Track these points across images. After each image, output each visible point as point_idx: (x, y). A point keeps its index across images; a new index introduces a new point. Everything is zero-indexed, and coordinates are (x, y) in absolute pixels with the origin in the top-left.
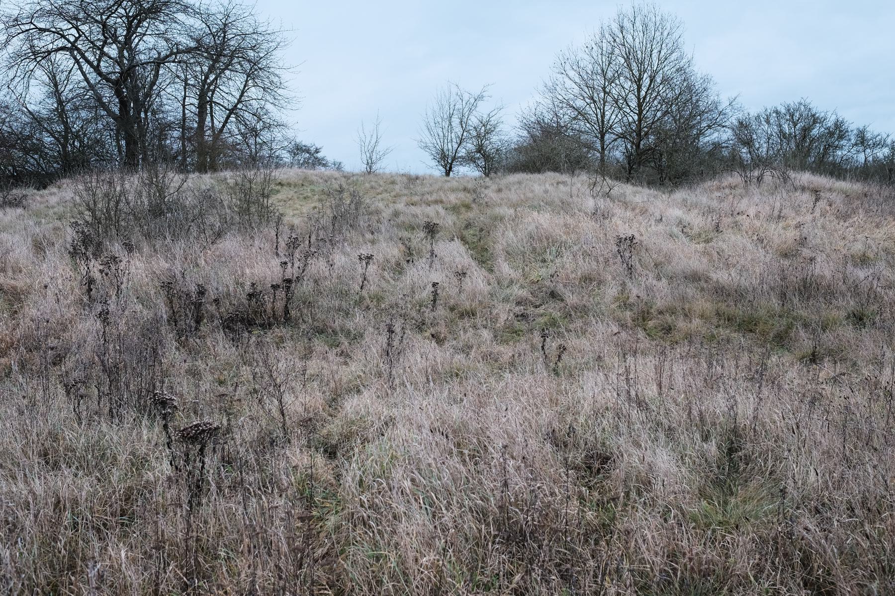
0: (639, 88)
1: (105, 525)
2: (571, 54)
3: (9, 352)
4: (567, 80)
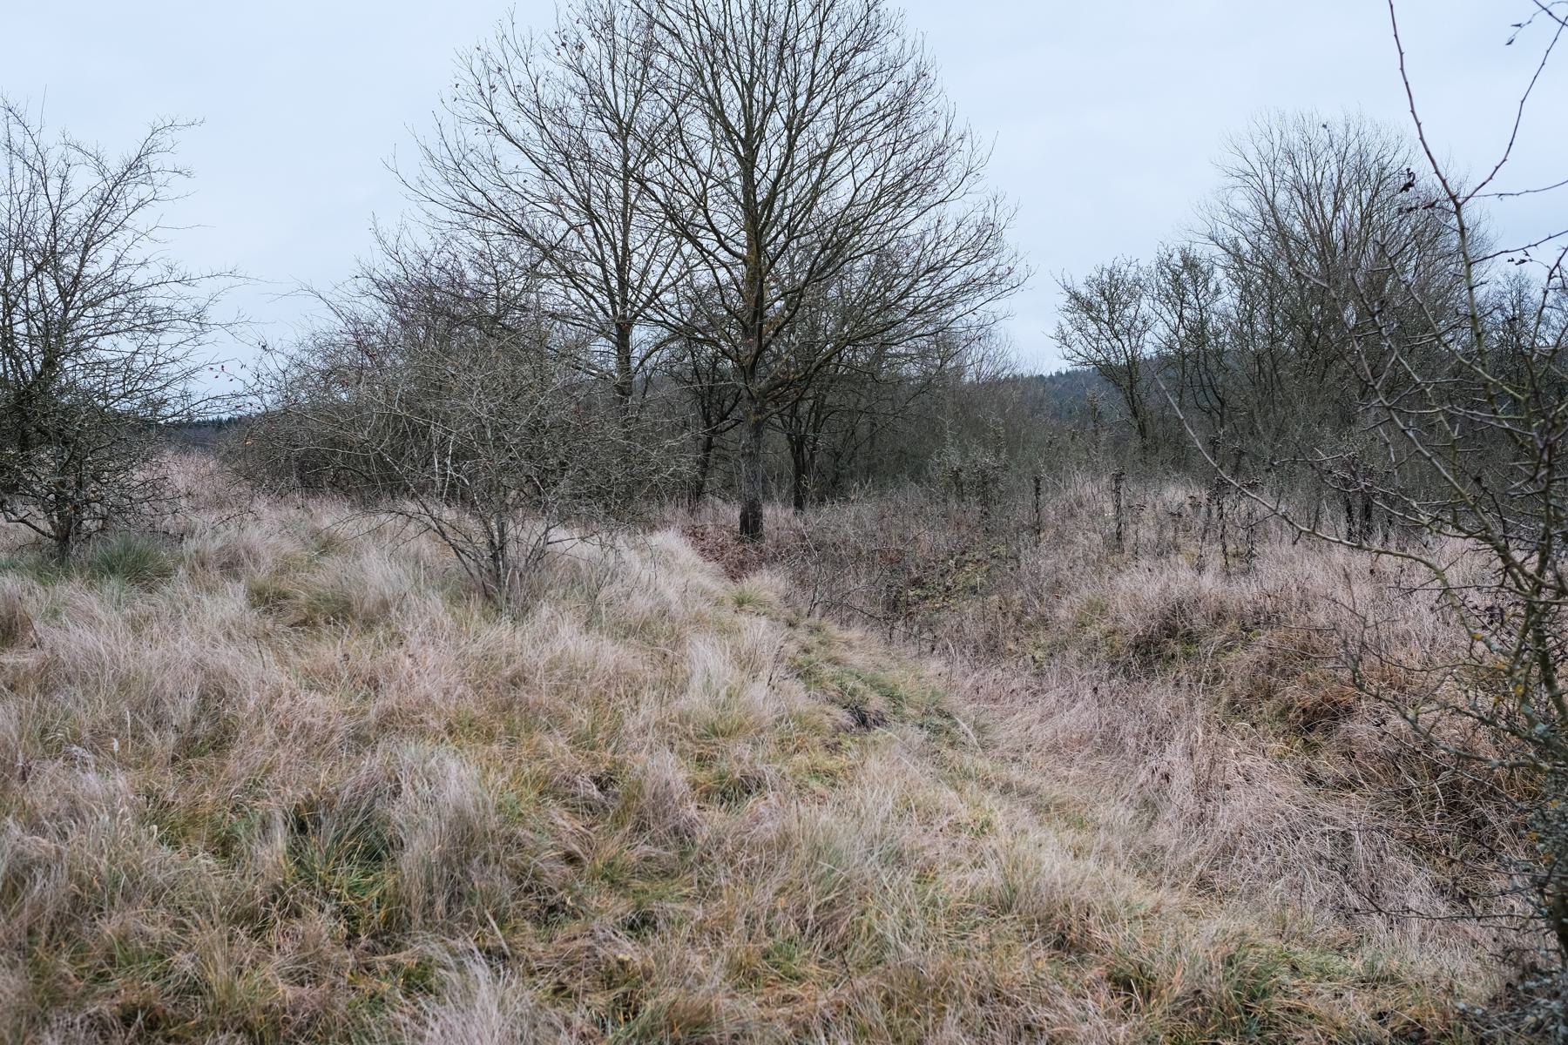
0: (748, 164)
1: (278, 947)
2: (511, 53)
3: (848, 819)
4: (503, 147)
